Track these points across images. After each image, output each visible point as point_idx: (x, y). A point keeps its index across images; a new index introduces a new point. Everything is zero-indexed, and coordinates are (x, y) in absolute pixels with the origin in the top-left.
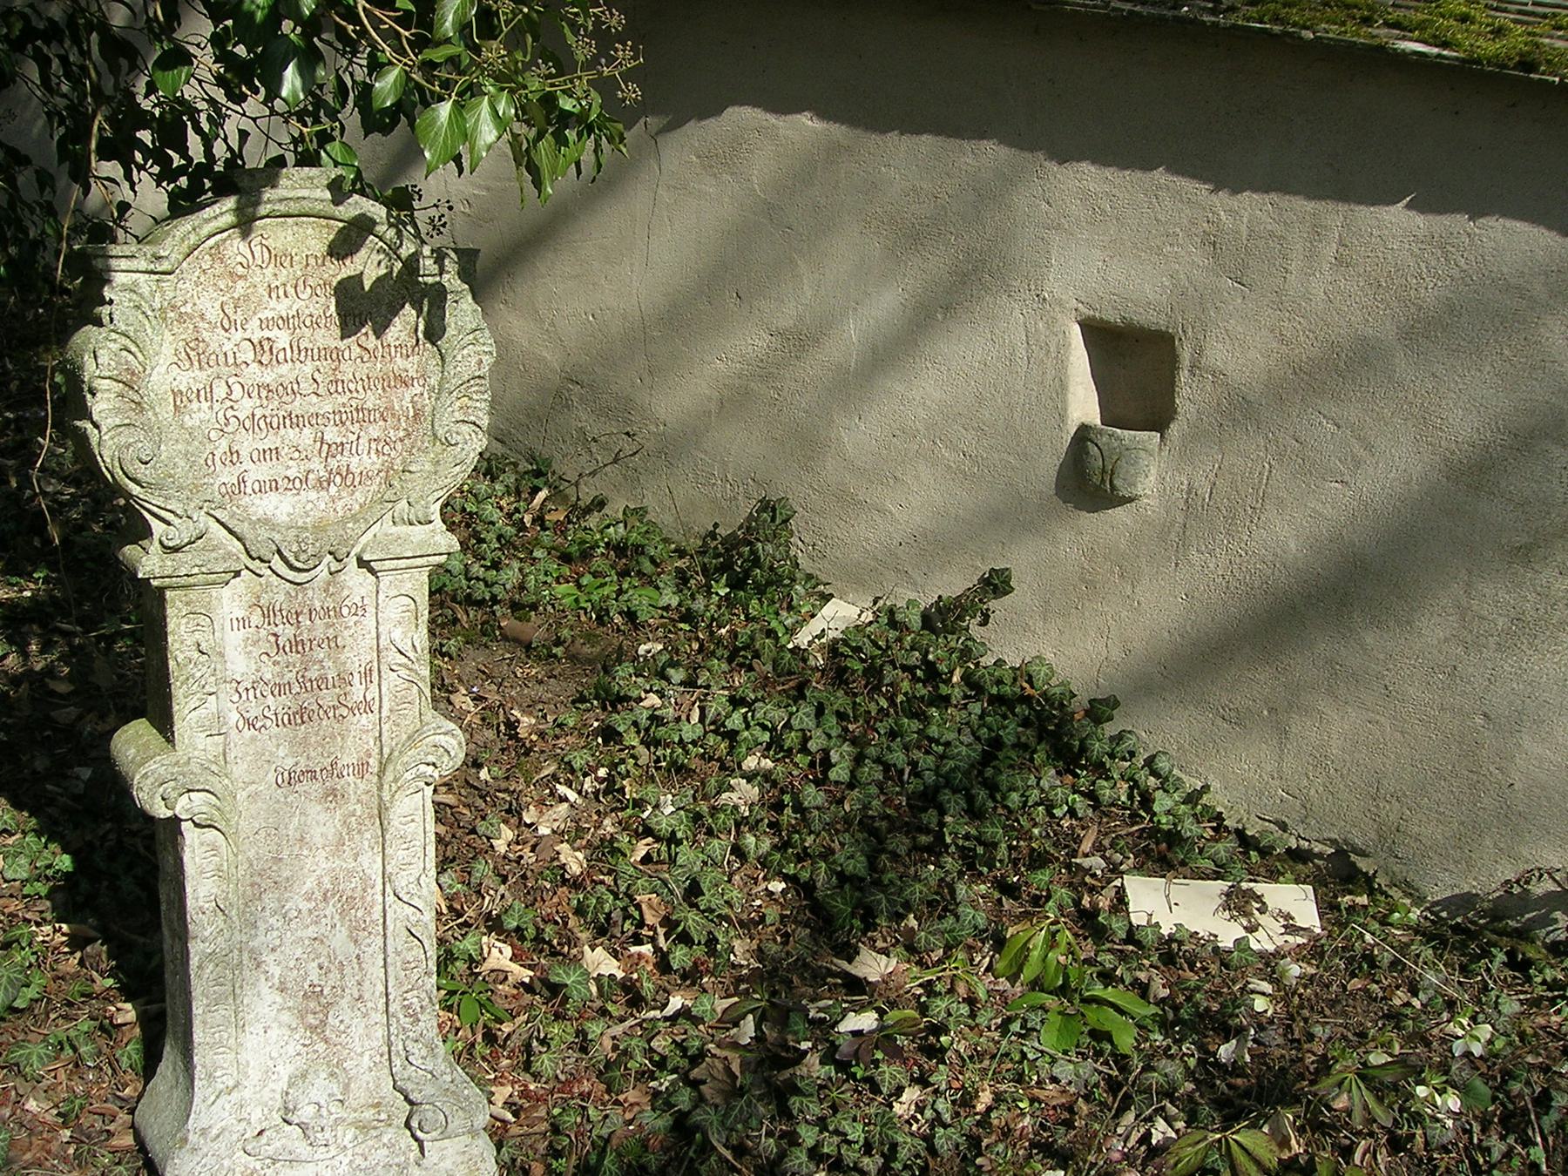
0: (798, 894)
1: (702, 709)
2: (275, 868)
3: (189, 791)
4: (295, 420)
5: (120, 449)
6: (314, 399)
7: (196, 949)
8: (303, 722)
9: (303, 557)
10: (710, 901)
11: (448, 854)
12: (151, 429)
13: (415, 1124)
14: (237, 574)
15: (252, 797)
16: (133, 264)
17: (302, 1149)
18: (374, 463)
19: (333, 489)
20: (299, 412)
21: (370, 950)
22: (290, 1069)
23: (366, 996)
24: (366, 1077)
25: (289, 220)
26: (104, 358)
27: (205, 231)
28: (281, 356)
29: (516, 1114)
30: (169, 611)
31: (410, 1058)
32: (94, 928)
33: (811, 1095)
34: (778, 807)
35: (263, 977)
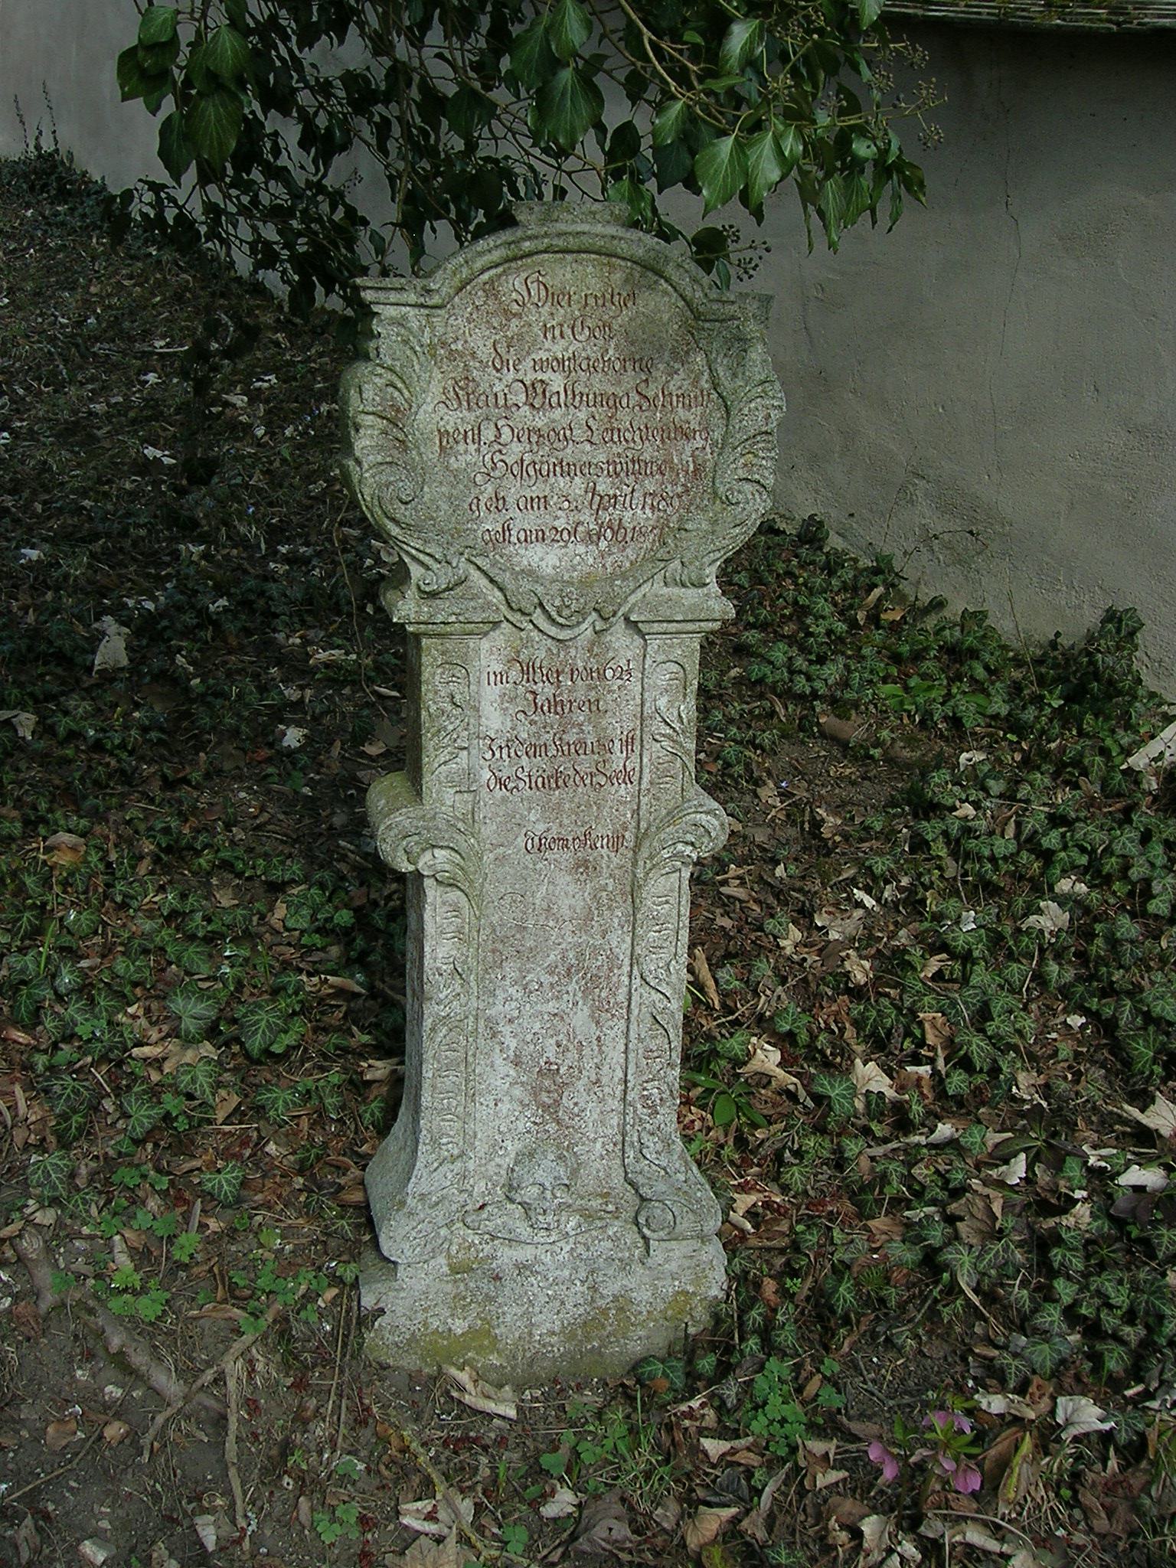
0: (1099, 1032)
1: (1018, 824)
2: (518, 936)
3: (434, 846)
4: (566, 469)
5: (379, 486)
6: (588, 447)
7: (432, 1011)
8: (558, 787)
9: (566, 612)
10: (998, 1028)
11: (731, 948)
12: (414, 469)
13: (642, 1220)
14: (496, 624)
15: (500, 860)
16: (404, 297)
17: (523, 1230)
18: (648, 519)
19: (603, 544)
20: (571, 460)
21: (612, 1033)
22: (518, 1145)
23: (604, 1080)
24: (596, 1165)
25: (569, 257)
26: (369, 394)
27: (479, 264)
28: (554, 399)
29: (756, 1226)
30: (424, 659)
31: (644, 1151)
32: (360, 984)
33: (1076, 1249)
34: (1090, 936)
35: (497, 1048)
